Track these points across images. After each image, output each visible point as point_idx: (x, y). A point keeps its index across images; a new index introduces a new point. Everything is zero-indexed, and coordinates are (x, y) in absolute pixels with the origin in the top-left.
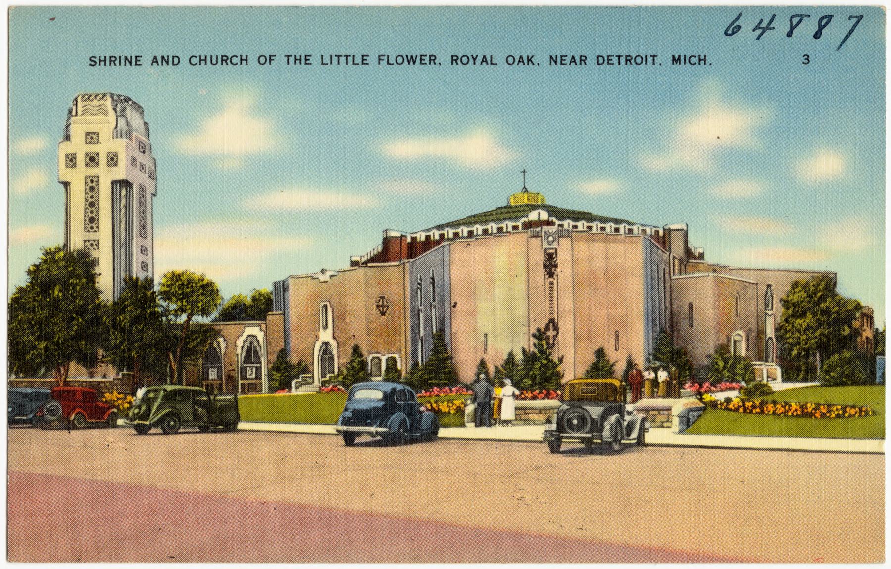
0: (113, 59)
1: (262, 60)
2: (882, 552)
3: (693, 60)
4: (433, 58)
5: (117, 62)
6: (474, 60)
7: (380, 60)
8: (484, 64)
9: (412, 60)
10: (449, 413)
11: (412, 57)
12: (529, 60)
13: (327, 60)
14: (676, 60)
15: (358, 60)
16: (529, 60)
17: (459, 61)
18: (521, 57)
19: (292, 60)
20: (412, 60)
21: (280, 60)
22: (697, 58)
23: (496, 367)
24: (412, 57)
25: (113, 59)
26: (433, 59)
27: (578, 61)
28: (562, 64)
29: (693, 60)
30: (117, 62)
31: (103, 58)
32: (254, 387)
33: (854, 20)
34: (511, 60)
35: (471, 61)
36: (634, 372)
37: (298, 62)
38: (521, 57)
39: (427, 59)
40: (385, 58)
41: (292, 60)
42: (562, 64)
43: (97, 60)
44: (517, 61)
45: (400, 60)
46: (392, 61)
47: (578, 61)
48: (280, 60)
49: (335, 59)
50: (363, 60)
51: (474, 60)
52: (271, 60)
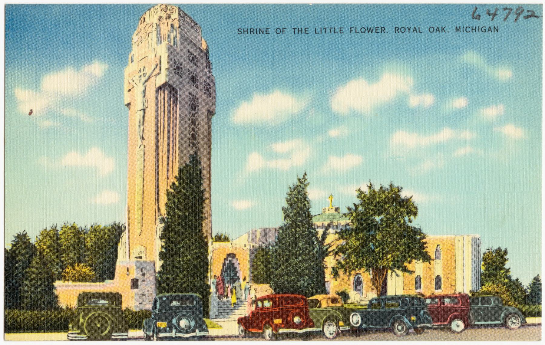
0: (252, 30)
1: (278, 31)
3: (468, 29)
4: (383, 29)
5: (255, 32)
6: (409, 30)
8: (438, 32)
9: (370, 30)
10: (374, 251)
12: (443, 29)
13: (318, 30)
15: (338, 30)
16: (443, 29)
17: (399, 30)
18: (438, 28)
19: (296, 31)
20: (370, 30)
23: (298, 205)
26: (458, 29)
27: (493, 29)
28: (305, 33)
29: (468, 29)
30: (255, 32)
31: (245, 30)
32: (115, 298)
34: (432, 30)
35: (407, 30)
38: (438, 28)
39: (379, 30)
42: (305, 33)
43: (242, 31)
44: (435, 30)
45: (363, 30)
46: (358, 30)
47: (493, 29)
49: (323, 30)
51: (409, 30)
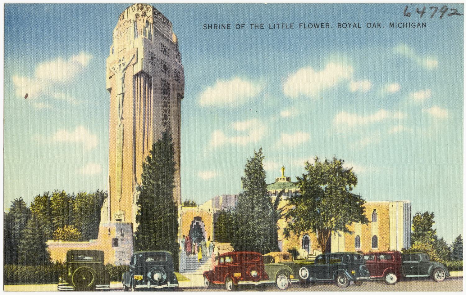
1: (238, 26)
2: (4, 6)
4: (327, 25)
5: (218, 28)
6: (350, 25)
7: (300, 26)
9: (316, 26)
11: (317, 24)
12: (379, 25)
13: (272, 26)
14: (391, 25)
15: (289, 26)
16: (379, 25)
18: (374, 24)
19: (253, 26)
20: (316, 26)
21: (247, 26)
22: (403, 24)
24: (317, 24)
25: (215, 26)
26: (328, 25)
28: (261, 28)
29: (401, 25)
30: (218, 28)
33: (434, 10)
35: (348, 25)
36: (366, 258)
37: (257, 28)
40: (303, 25)
41: (253, 26)
42: (261, 28)
43: (207, 26)
44: (372, 26)
45: (310, 26)
46: (306, 26)
48: (247, 26)
49: (276, 26)
50: (291, 26)
51: (350, 25)
52: (242, 27)
